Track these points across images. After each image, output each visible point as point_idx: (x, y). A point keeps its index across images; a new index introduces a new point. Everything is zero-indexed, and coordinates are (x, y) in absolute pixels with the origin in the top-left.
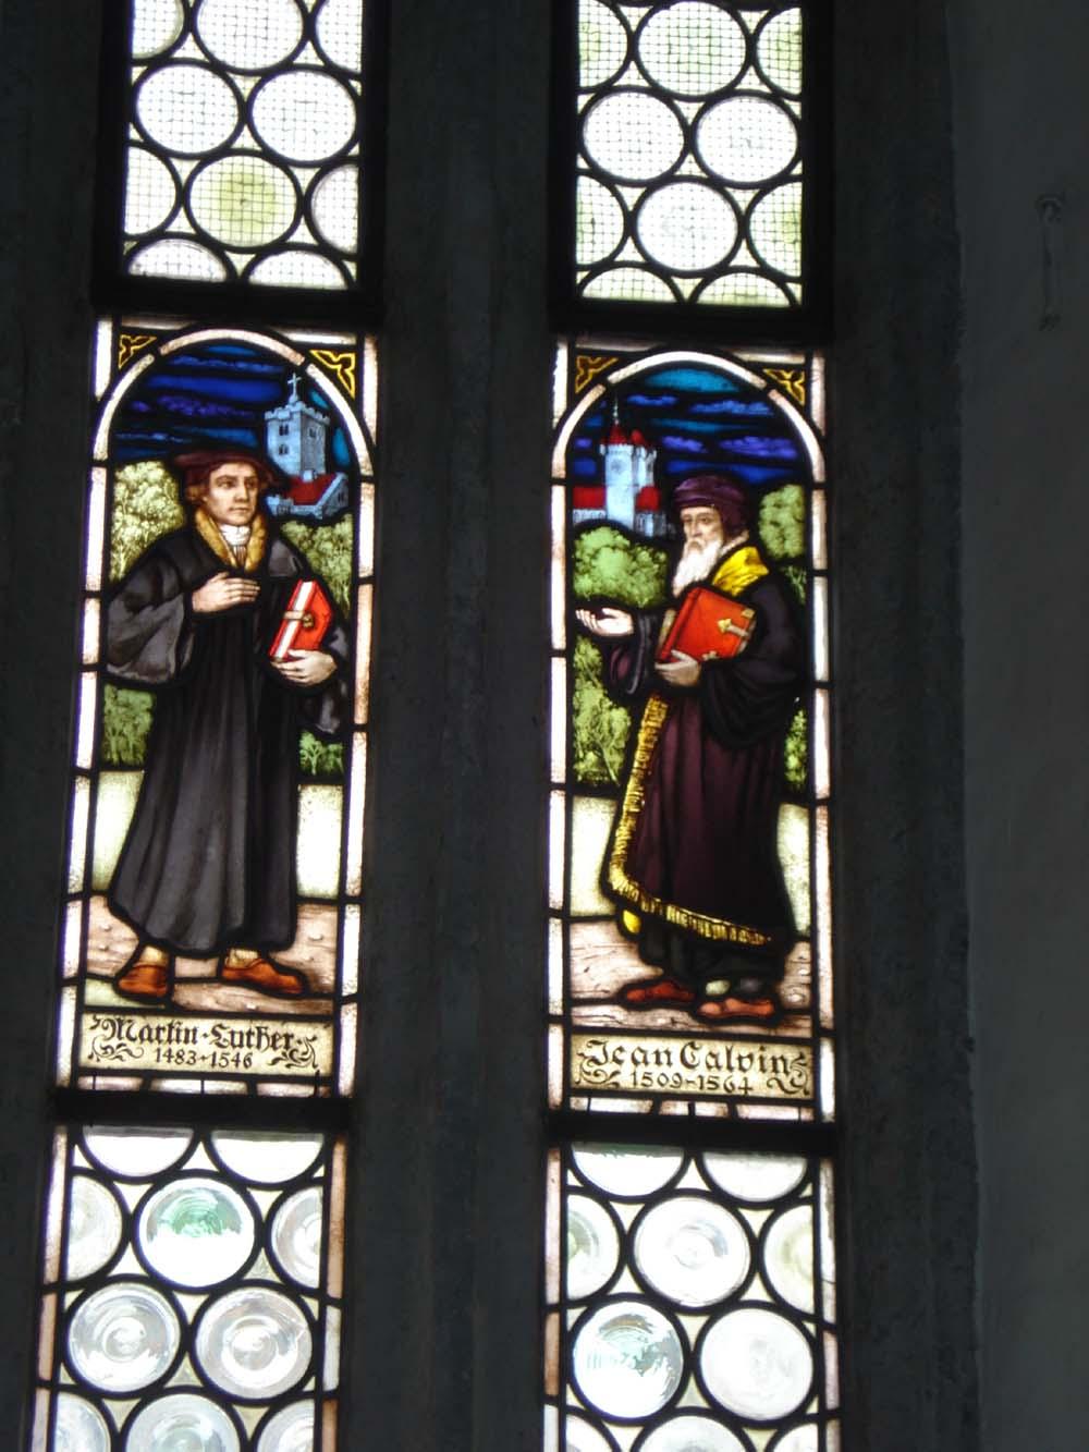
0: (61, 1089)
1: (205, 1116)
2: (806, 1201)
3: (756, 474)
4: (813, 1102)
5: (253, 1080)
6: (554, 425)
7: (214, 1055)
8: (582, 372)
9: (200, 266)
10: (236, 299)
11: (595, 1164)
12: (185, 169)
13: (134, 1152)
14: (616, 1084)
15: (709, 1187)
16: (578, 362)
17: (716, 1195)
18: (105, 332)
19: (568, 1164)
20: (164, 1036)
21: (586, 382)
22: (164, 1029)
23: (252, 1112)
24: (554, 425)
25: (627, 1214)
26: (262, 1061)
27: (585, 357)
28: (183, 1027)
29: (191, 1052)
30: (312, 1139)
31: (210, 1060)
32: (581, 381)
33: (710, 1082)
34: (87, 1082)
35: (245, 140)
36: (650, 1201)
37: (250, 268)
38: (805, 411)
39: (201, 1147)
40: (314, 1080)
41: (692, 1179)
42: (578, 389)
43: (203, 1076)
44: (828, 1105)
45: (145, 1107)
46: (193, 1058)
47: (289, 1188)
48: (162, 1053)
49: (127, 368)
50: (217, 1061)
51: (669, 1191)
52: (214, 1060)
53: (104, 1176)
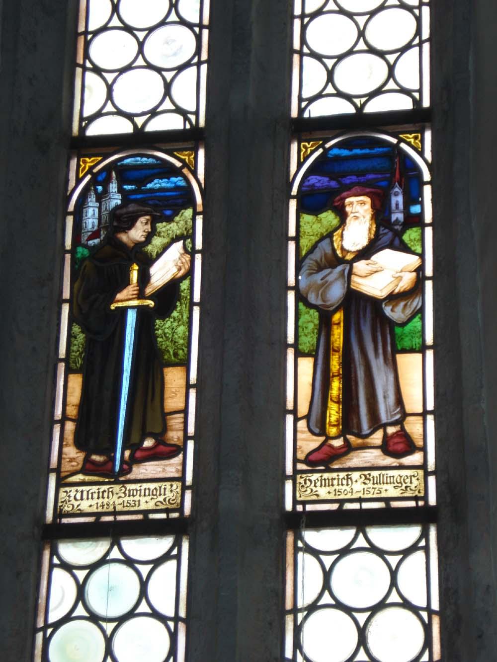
0: (288, 512)
1: (361, 520)
2: (421, 548)
3: (132, 208)
4: (425, 498)
5: (387, 500)
6: (291, 181)
7: (364, 489)
8: (304, 150)
9: (123, 127)
10: (140, 139)
11: (311, 537)
12: (169, 76)
13: (76, 552)
14: (79, 510)
15: (370, 546)
16: (302, 146)
17: (373, 549)
18: (294, 147)
19: (54, 552)
20: (95, 496)
21: (86, 171)
22: (335, 479)
23: (390, 516)
24: (291, 181)
25: (328, 561)
26: (392, 492)
27: (304, 143)
28: (143, 488)
29: (133, 501)
30: (352, 529)
31: (95, 506)
32: (83, 171)
33: (367, 491)
34: (65, 521)
35: (140, 62)
36: (93, 568)
37: (363, 105)
38: (421, 154)
39: (361, 535)
40: (416, 499)
41: (361, 542)
42: (81, 175)
43: (360, 500)
44: (187, 510)
45: (337, 518)
46: (135, 503)
47: (406, 553)
48: (99, 505)
49: (306, 158)
50: (125, 505)
51: (103, 561)
52: (364, 491)
53: (67, 567)
